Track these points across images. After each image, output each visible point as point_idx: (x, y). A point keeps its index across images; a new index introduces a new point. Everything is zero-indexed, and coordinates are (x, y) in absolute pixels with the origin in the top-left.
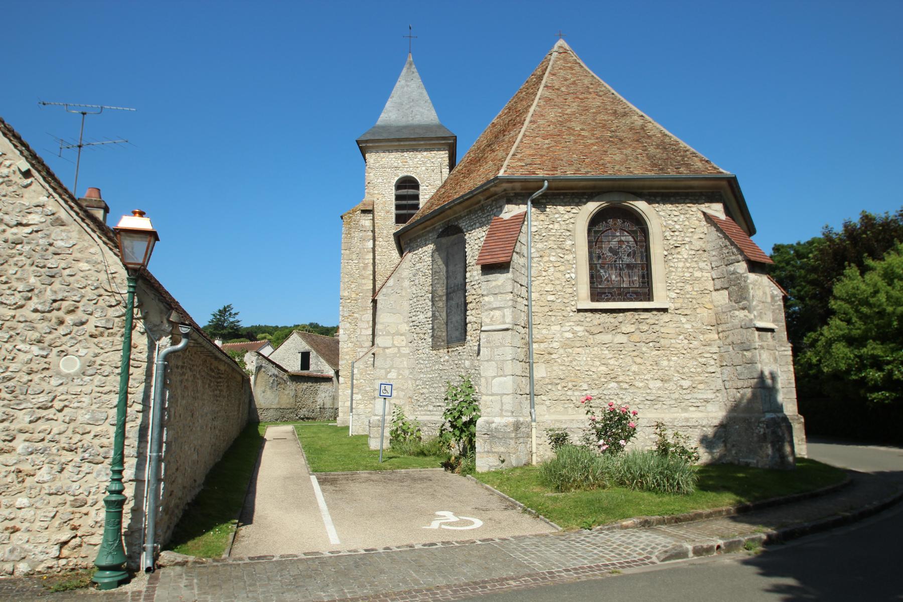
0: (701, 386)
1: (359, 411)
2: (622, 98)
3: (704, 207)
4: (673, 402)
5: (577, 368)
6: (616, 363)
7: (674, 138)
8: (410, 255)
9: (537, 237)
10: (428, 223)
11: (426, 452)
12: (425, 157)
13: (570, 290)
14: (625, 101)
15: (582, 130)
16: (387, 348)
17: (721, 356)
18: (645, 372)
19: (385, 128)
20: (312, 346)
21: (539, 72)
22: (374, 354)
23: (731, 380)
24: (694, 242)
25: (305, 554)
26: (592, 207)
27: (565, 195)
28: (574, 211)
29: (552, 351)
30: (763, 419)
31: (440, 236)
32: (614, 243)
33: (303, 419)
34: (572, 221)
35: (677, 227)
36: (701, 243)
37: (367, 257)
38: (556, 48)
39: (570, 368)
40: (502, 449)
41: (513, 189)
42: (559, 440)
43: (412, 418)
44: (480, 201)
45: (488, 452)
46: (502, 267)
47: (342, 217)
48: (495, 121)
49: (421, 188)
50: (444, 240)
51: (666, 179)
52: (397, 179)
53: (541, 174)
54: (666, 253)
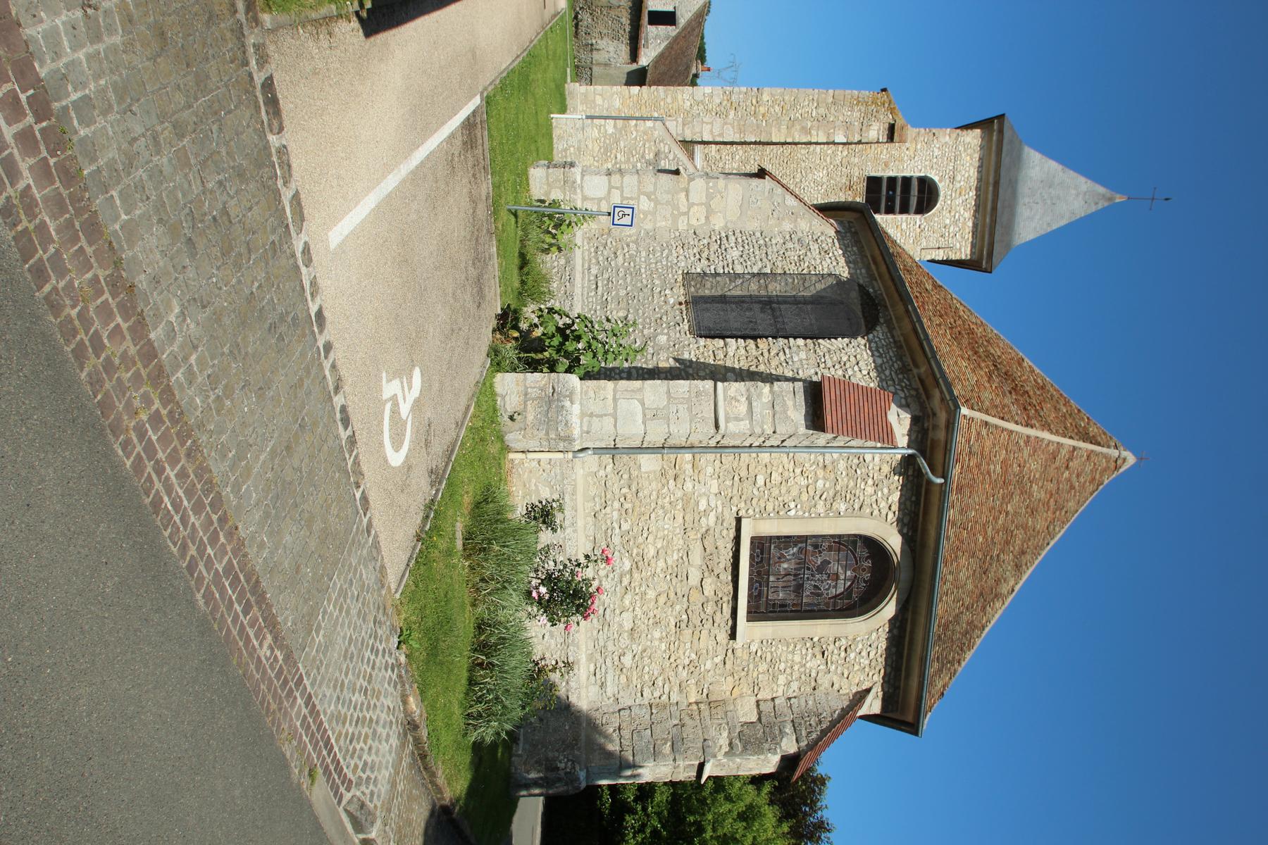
0: (623, 679)
1: (589, 130)
2: (1040, 558)
3: (877, 691)
4: (602, 644)
5: (653, 516)
6: (658, 570)
7: (978, 641)
8: (832, 233)
9: (856, 461)
10: (883, 268)
11: (526, 270)
12: (964, 223)
13: (770, 508)
14: (1037, 562)
15: (1007, 513)
16: (687, 196)
17: (665, 707)
18: (645, 608)
19: (1017, 160)
20: (684, 29)
21: (1093, 430)
22: (677, 172)
23: (632, 720)
24: (828, 676)
25: (296, 197)
26: (894, 541)
27: (917, 503)
28: (890, 515)
29: (680, 480)
30: (578, 768)
31: (861, 288)
32: (834, 567)
33: (576, 17)
34: (876, 512)
35: (852, 655)
36: (827, 684)
37: (820, 133)
38: (1125, 454)
39: (653, 505)
40: (530, 417)
41: (935, 427)
42: (544, 515)
43: (578, 241)
44: (917, 366)
45: (526, 394)
46: (816, 419)
47: (884, 90)
48: (1028, 362)
49: (918, 217)
50: (854, 295)
51: (925, 648)
52: (936, 179)
53: (956, 471)
54: (815, 639)
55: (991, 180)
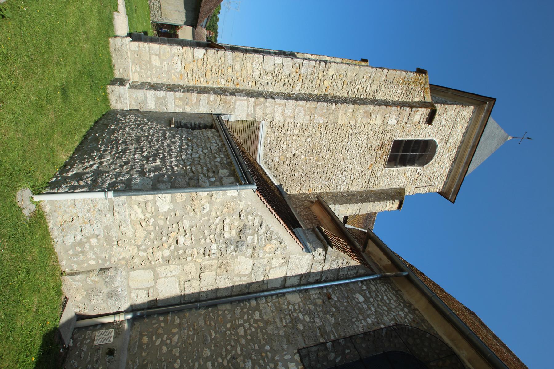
52: (437, 141)
55: (471, 144)
